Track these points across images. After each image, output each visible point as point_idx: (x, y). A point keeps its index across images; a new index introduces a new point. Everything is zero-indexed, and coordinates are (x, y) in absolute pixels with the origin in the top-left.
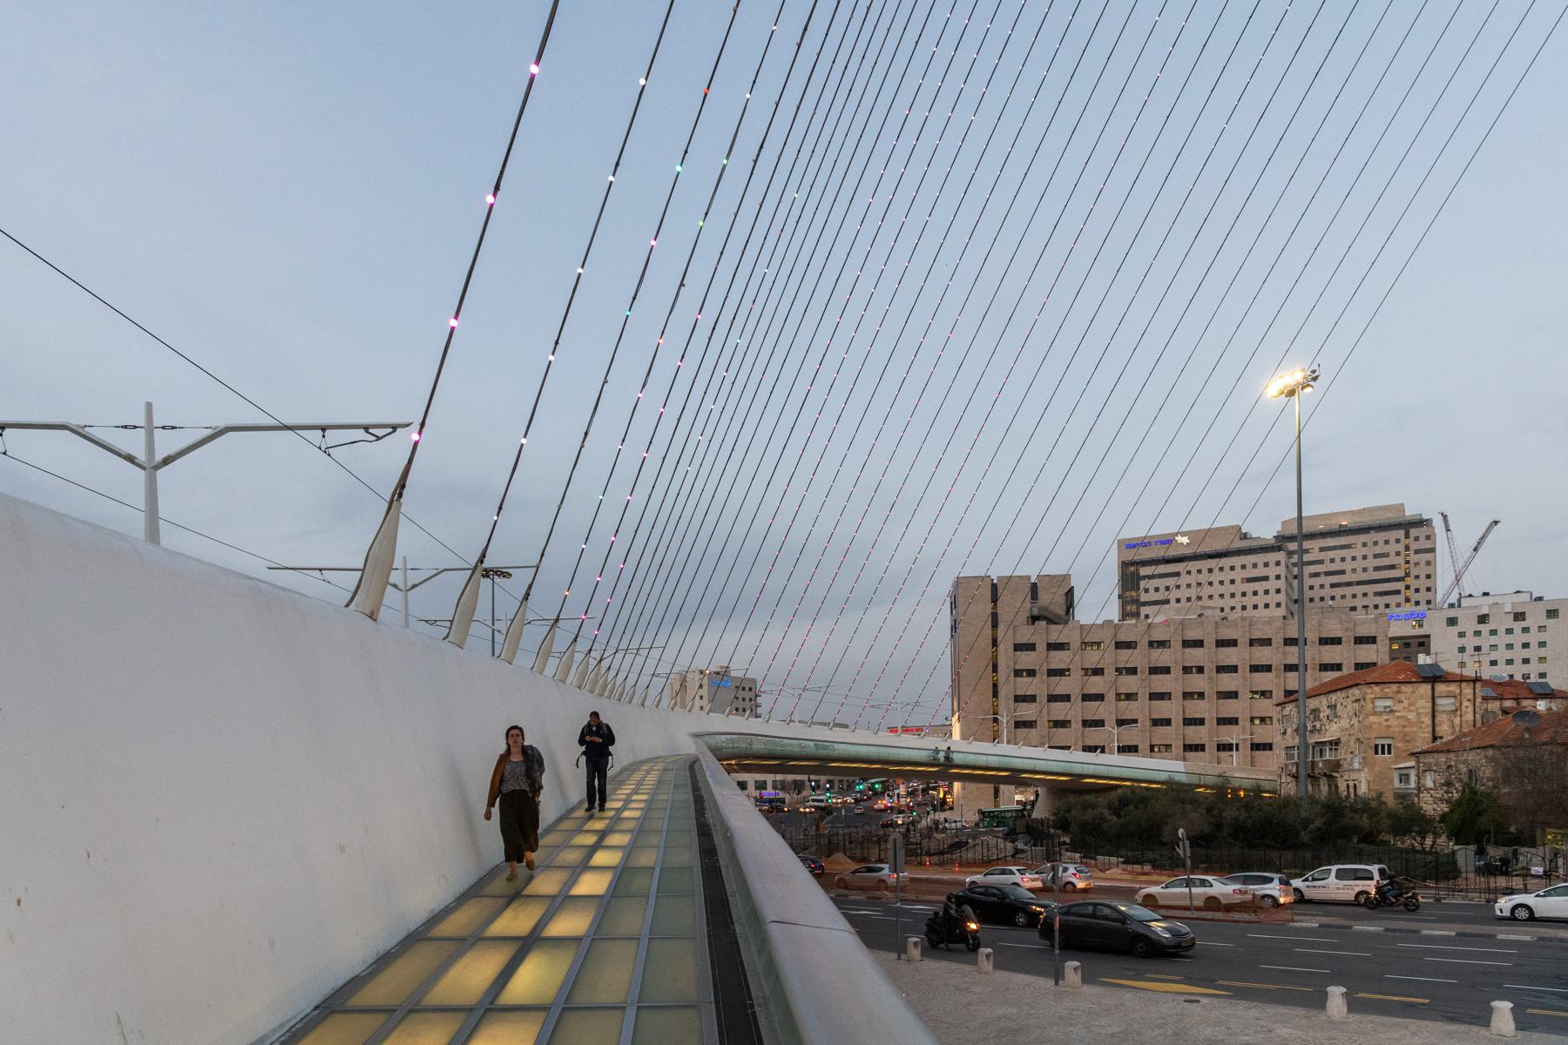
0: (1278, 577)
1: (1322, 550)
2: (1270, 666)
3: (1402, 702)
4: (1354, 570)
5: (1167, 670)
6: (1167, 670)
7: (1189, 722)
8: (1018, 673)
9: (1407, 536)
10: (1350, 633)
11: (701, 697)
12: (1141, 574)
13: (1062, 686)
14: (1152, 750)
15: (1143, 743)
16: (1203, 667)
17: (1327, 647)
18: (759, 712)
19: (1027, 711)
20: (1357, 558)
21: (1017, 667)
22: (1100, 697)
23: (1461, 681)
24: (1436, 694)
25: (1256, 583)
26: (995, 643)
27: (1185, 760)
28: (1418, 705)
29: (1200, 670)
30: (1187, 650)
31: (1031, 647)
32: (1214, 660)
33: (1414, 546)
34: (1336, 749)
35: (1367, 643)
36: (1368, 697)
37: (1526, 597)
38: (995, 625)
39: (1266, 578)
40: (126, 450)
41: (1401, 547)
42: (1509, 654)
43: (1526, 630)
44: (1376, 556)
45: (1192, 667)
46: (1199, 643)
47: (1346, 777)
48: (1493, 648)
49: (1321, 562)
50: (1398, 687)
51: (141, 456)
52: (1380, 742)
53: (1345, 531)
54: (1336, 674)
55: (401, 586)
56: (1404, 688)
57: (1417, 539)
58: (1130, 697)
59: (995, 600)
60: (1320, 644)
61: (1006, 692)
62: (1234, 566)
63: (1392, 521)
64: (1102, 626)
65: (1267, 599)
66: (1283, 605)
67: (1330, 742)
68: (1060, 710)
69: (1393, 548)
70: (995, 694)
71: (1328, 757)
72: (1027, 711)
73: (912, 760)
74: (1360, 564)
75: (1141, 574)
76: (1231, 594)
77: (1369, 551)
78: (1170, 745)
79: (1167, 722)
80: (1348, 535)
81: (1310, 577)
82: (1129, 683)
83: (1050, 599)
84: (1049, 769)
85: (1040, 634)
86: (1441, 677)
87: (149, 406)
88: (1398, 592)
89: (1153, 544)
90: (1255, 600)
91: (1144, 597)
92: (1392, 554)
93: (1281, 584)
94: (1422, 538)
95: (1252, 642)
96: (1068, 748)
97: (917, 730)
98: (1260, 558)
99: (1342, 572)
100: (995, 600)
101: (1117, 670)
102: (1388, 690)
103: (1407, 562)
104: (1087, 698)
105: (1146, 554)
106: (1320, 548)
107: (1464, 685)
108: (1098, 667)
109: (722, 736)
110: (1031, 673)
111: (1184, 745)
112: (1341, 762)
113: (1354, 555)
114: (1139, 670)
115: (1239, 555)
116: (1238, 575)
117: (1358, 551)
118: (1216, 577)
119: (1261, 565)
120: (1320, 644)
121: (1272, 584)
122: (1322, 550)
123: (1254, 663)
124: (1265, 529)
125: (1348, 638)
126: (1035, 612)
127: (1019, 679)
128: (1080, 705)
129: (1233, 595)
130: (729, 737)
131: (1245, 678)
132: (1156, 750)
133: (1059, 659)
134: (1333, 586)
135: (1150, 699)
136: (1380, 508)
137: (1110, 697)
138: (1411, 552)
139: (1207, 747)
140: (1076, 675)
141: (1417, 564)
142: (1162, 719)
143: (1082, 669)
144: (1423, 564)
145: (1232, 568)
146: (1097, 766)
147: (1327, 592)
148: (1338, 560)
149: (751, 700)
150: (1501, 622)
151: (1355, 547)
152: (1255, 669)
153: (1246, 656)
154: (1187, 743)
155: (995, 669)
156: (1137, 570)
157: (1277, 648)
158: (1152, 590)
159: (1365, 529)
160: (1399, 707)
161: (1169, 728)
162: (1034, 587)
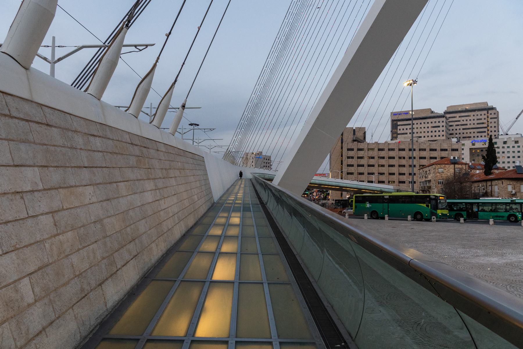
0: (443, 126)
1: (460, 117)
2: (426, 157)
3: (446, 170)
4: (470, 124)
5: (394, 158)
6: (394, 158)
7: (400, 174)
8: (348, 158)
9: (488, 113)
10: (450, 148)
11: (252, 166)
13: (362, 162)
15: (386, 180)
16: (405, 157)
17: (443, 152)
19: (351, 170)
20: (471, 120)
21: (348, 156)
22: (373, 166)
23: (462, 164)
24: (455, 168)
26: (342, 148)
28: (450, 171)
29: (404, 158)
30: (400, 152)
31: (352, 150)
32: (408, 155)
33: (490, 116)
34: (430, 183)
35: (455, 151)
36: (437, 168)
37: (520, 136)
38: (342, 143)
39: (439, 127)
40: (146, 112)
41: (486, 117)
42: (513, 155)
43: (519, 147)
44: (478, 120)
45: (401, 157)
46: (403, 150)
47: (432, 191)
48: (508, 152)
49: (459, 121)
51: (49, 58)
52: (439, 181)
53: (467, 111)
54: (435, 160)
55: (149, 114)
56: (446, 166)
57: (491, 114)
58: (361, 158)
60: (441, 151)
61: (345, 163)
62: (428, 122)
63: (483, 108)
64: (374, 144)
65: (439, 133)
66: (445, 136)
67: (428, 181)
68: (361, 170)
69: (483, 117)
70: (342, 164)
71: (427, 185)
72: (351, 170)
74: (472, 122)
76: (428, 131)
78: (395, 181)
79: (394, 174)
80: (468, 112)
81: (456, 126)
82: (382, 162)
83: (359, 135)
84: (351, 187)
85: (355, 145)
86: (457, 163)
87: (151, 103)
88: (485, 132)
89: (402, 114)
90: (435, 134)
91: (399, 132)
92: (483, 119)
93: (444, 128)
94: (493, 114)
95: (420, 150)
96: (363, 181)
97: (324, 175)
98: (437, 120)
99: (466, 125)
101: (379, 157)
102: (442, 166)
103: (488, 122)
104: (369, 166)
105: (401, 117)
106: (459, 116)
107: (463, 165)
109: (258, 174)
110: (352, 158)
111: (399, 181)
112: (431, 187)
113: (470, 119)
114: (385, 157)
115: (430, 119)
116: (430, 125)
117: (472, 118)
118: (423, 126)
119: (437, 122)
120: (441, 151)
121: (441, 129)
122: (460, 117)
123: (420, 156)
124: (440, 110)
125: (438, 149)
126: (354, 139)
127: (349, 159)
128: (367, 168)
129: (428, 132)
130: (259, 174)
132: (390, 183)
133: (361, 154)
134: (463, 129)
135: (389, 167)
136: (479, 103)
137: (376, 166)
138: (489, 118)
139: (406, 182)
141: (491, 123)
142: (392, 173)
143: (368, 157)
144: (493, 122)
145: (428, 123)
147: (462, 131)
148: (465, 120)
149: (269, 167)
150: (511, 144)
151: (471, 116)
152: (421, 158)
153: (366, 154)
154: (400, 181)
155: (342, 156)
157: (427, 152)
159: (474, 110)
160: (445, 171)
162: (354, 130)
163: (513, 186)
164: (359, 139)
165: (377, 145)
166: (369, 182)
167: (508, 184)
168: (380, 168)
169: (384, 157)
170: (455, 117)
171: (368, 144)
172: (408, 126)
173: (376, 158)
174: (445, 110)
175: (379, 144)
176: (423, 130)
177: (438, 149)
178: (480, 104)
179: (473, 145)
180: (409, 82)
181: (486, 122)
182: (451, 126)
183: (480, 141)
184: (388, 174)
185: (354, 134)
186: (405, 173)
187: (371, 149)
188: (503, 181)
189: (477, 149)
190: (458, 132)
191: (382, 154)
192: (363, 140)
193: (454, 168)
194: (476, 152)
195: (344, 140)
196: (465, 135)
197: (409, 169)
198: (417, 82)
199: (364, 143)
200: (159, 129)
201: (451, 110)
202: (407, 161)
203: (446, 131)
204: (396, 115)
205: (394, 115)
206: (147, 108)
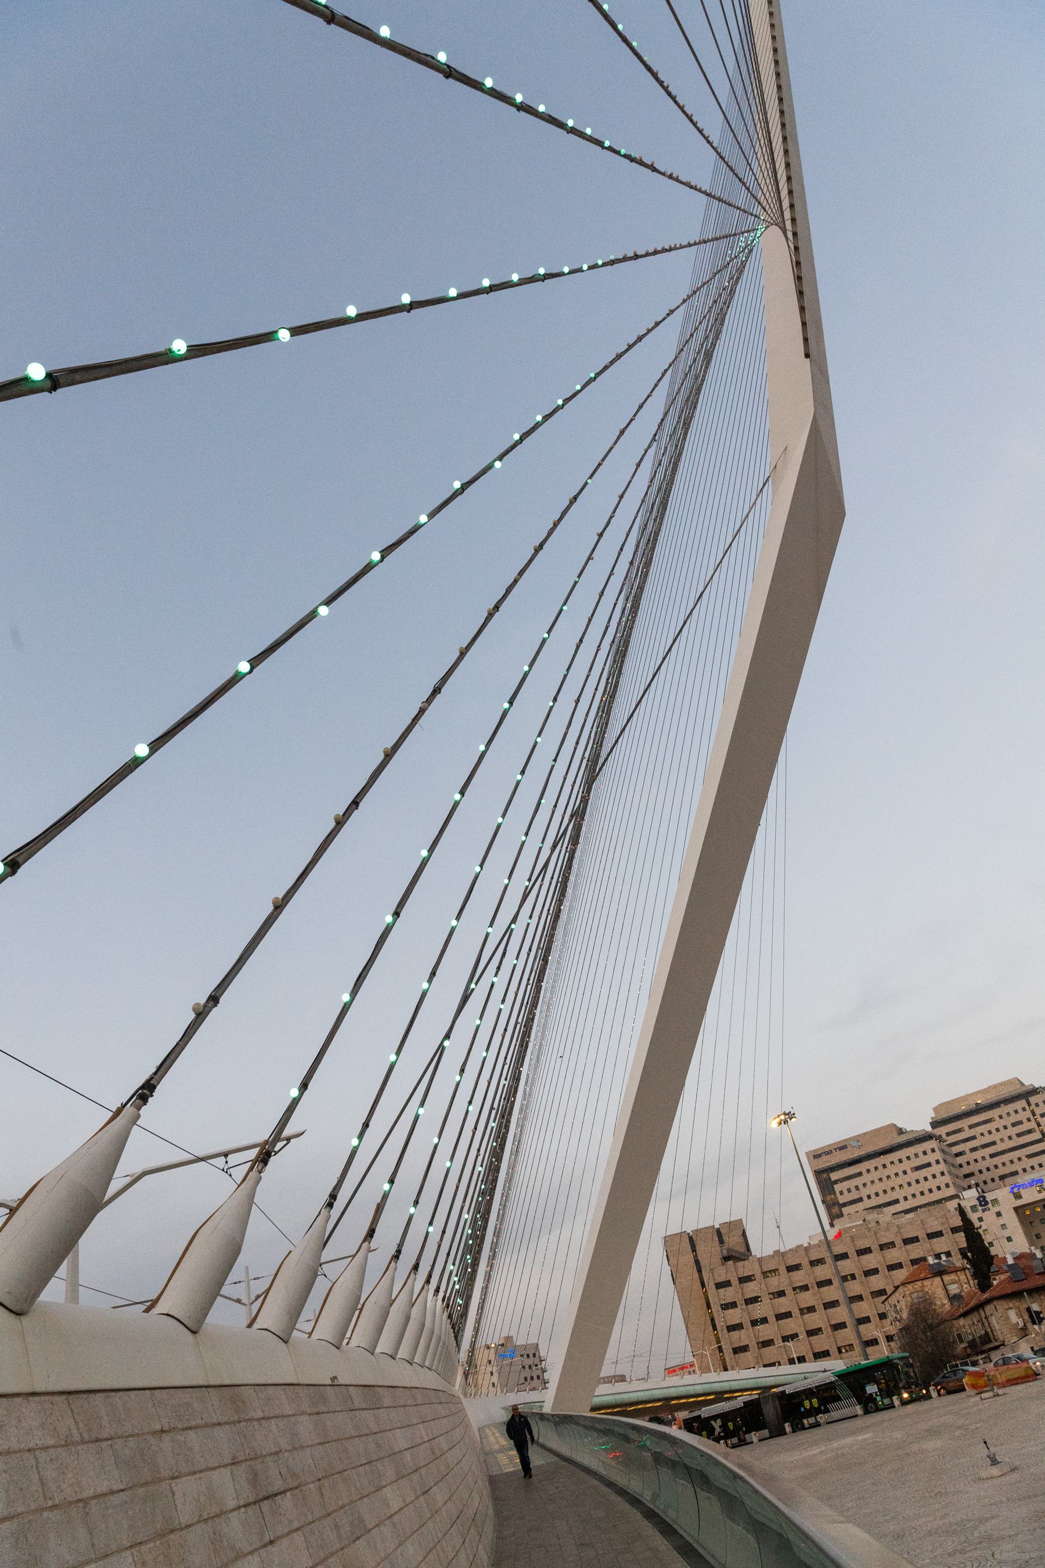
1: (971, 1127)
9: (1029, 1104)
12: (833, 1180)
13: (759, 1311)
14: (840, 1352)
15: (807, 1353)
18: (546, 1377)
24: (945, 1283)
25: (923, 1170)
26: (703, 1285)
27: (841, 1359)
38: (699, 1271)
39: (929, 1165)
41: (1028, 1114)
44: (1014, 1125)
49: (974, 1138)
50: (922, 1283)
53: (982, 1108)
56: (925, 1283)
58: (754, 1300)
59: (694, 1250)
61: (720, 1324)
64: (773, 1257)
66: (951, 1185)
70: (714, 1328)
73: (640, 1399)
75: (833, 1180)
77: (1008, 1121)
78: (852, 1345)
83: (733, 1241)
86: (944, 1271)
87: (247, 1268)
91: (842, 1200)
98: (919, 1148)
100: (694, 1250)
101: (794, 1289)
108: (780, 1289)
116: (907, 1165)
118: (891, 1170)
121: (936, 1169)
122: (971, 1127)
124: (919, 1122)
131: (886, 1277)
132: (843, 1351)
134: (992, 1156)
135: (825, 1309)
136: (1001, 1084)
140: (766, 1300)
143: (769, 1294)
145: (900, 1161)
146: (777, 1378)
149: (538, 1377)
151: (995, 1121)
155: (709, 1307)
156: (829, 1175)
158: (845, 1192)
159: (996, 1104)
161: (846, 1330)
162: (719, 1232)
163: (1017, 1310)
164: (736, 1251)
165: (781, 1258)
166: (791, 1361)
167: (1007, 1309)
168: (806, 1316)
169: (807, 1285)
170: (959, 1131)
171: (760, 1260)
172: (857, 1179)
173: (789, 1291)
174: (932, 1118)
175: (783, 1254)
176: (895, 1182)
177: (922, 1235)
178: (1002, 1085)
179: (1018, 1196)
180: (778, 1120)
181: (1036, 1126)
182: (957, 1155)
183: (1029, 1183)
184: (829, 1329)
185: (721, 1241)
186: (868, 1317)
187: (770, 1271)
188: (995, 1303)
189: (1034, 1206)
190: (982, 1165)
191: (800, 1278)
192: (746, 1253)
193: (943, 1283)
194: (1033, 1212)
195: (703, 1263)
196: (1002, 1171)
197: (874, 1302)
198: (794, 1114)
199: (748, 1259)
200: (411, 1365)
201: (945, 1115)
202: (862, 1282)
203: (950, 1172)
204: (820, 1156)
205: (815, 1157)
206: (235, 1283)
